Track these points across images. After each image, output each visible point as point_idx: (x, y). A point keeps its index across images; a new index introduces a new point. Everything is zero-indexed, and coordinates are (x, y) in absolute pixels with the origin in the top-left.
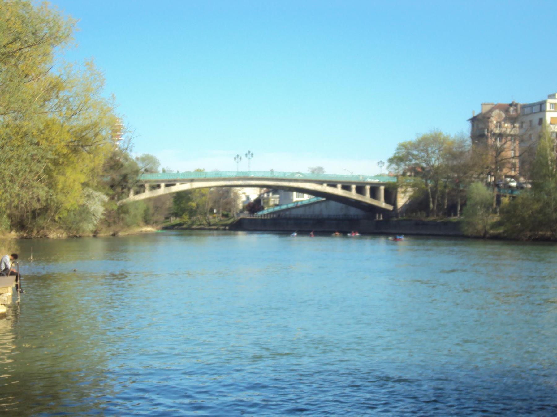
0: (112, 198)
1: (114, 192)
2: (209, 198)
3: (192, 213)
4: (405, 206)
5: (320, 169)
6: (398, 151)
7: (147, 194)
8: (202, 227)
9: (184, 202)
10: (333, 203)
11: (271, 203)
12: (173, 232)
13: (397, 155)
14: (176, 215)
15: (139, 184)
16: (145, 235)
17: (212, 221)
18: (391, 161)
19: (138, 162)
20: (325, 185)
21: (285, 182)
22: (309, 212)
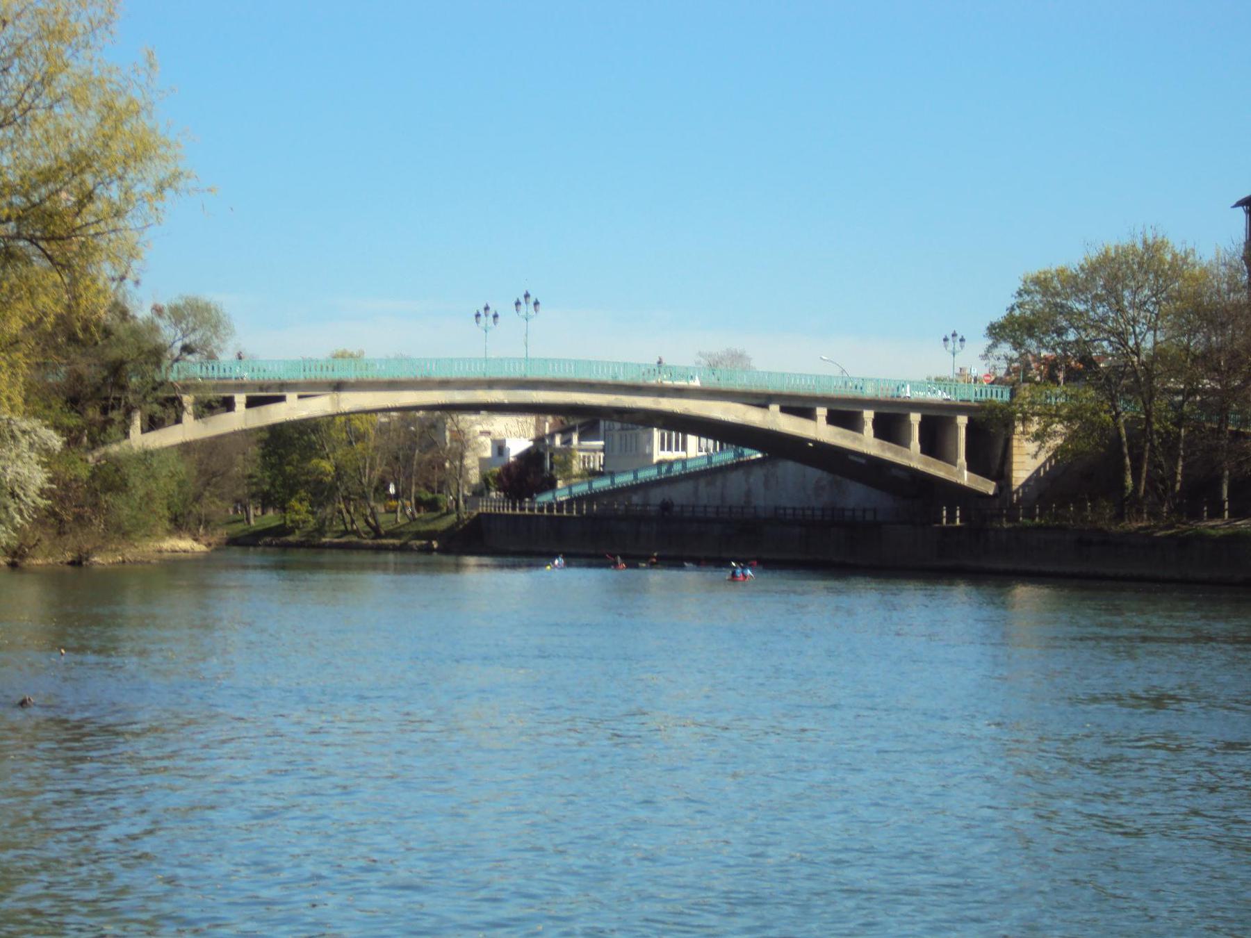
0: (72, 441)
1: (80, 422)
2: (376, 448)
3: (321, 493)
4: (1035, 478)
5: (737, 358)
6: (1020, 300)
7: (189, 429)
8: (354, 539)
9: (295, 457)
10: (789, 469)
11: (577, 467)
12: (253, 556)
13: (1017, 313)
14: (266, 501)
15: (161, 394)
16: (175, 566)
17: (385, 521)
18: (997, 332)
19: (161, 323)
20: (775, 408)
21: (643, 395)
22: (707, 495)
